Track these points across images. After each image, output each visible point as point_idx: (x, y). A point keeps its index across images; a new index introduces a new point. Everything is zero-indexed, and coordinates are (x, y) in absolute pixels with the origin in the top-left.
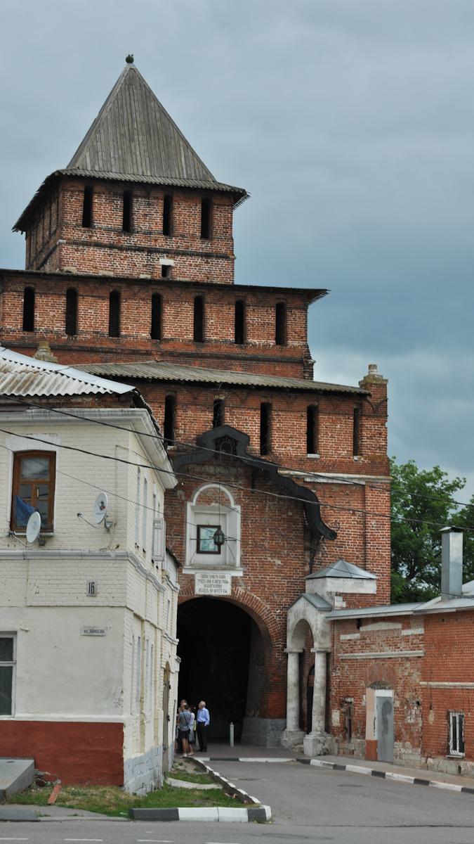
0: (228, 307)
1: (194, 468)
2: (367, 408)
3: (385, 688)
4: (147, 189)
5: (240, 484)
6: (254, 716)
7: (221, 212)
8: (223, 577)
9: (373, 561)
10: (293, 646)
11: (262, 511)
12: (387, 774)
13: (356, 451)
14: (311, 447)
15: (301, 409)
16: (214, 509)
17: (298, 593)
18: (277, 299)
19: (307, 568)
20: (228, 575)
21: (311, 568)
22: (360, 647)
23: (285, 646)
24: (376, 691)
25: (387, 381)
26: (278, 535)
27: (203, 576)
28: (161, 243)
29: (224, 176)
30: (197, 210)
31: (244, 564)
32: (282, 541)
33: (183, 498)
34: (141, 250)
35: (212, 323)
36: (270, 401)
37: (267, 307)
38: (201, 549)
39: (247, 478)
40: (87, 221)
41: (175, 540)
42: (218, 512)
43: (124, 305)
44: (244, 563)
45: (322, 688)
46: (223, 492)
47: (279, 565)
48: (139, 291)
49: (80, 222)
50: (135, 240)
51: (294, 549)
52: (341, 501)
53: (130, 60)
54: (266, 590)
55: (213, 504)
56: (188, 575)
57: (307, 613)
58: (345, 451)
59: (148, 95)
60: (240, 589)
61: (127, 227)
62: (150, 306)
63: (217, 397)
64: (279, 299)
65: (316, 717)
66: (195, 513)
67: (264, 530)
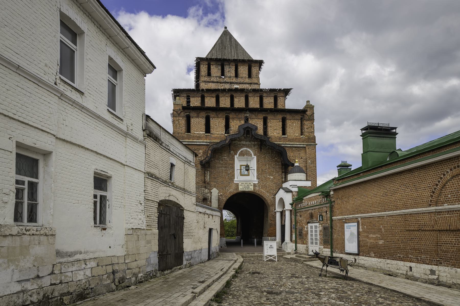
4: (229, 61)
8: (250, 183)
9: (310, 176)
10: (278, 209)
14: (284, 133)
19: (284, 180)
23: (275, 209)
28: (234, 80)
29: (255, 57)
34: (228, 83)
40: (209, 74)
43: (221, 99)
46: (249, 151)
49: (206, 75)
52: (296, 153)
59: (231, 37)
67: (266, 165)
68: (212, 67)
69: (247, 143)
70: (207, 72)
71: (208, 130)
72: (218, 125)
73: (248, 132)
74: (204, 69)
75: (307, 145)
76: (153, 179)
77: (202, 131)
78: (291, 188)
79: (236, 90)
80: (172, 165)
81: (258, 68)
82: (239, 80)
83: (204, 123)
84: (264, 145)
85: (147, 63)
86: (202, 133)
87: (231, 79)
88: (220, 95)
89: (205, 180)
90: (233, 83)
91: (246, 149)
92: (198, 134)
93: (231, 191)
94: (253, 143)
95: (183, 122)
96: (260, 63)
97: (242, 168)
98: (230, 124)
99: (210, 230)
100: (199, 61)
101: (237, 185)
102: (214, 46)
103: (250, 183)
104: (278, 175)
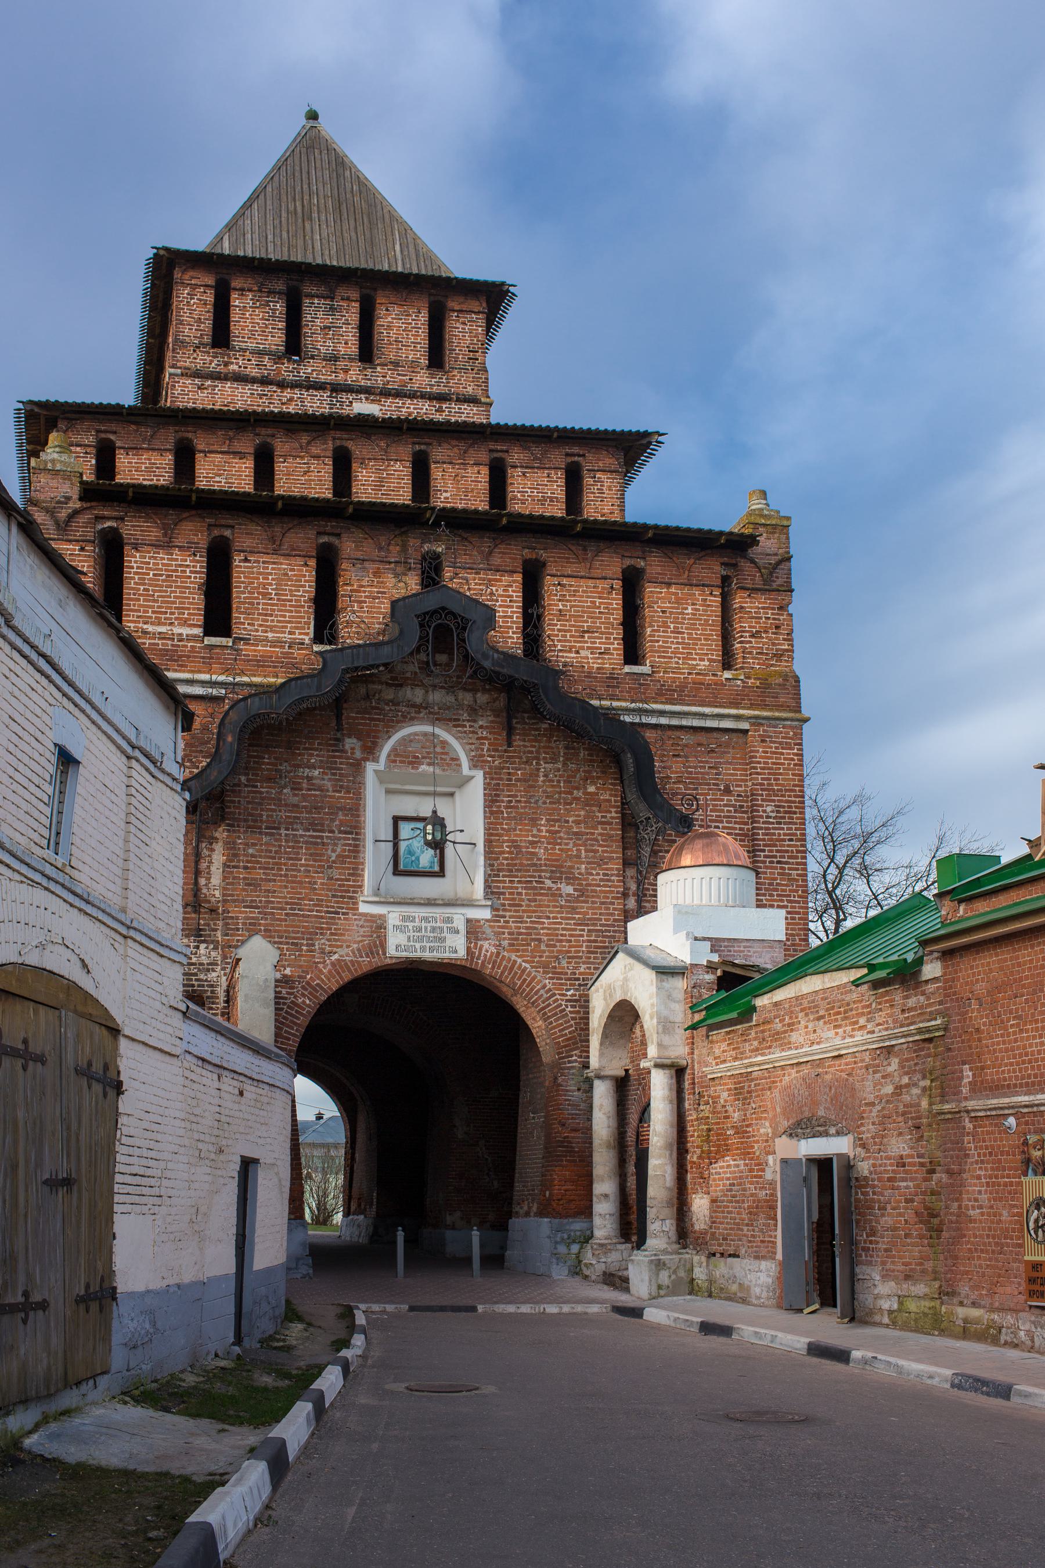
0: (476, 469)
1: (381, 691)
3: (826, 1134)
4: (332, 278)
5: (481, 727)
6: (527, 1214)
7: (464, 323)
8: (449, 920)
11: (529, 781)
12: (856, 1354)
13: (727, 662)
14: (632, 653)
15: (609, 573)
16: (424, 774)
17: (610, 944)
18: (567, 455)
19: (632, 903)
20: (459, 917)
21: (639, 901)
22: (755, 1043)
24: (803, 1142)
25: (788, 518)
26: (568, 833)
27: (405, 919)
28: (355, 375)
29: (460, 264)
31: (492, 893)
32: (575, 845)
33: (358, 754)
34: (320, 386)
35: (446, 498)
36: (543, 555)
37: (549, 468)
38: (401, 867)
39: (496, 713)
40: (221, 336)
41: (342, 842)
42: (431, 789)
45: (668, 1146)
46: (444, 743)
47: (569, 895)
48: (309, 443)
49: (207, 339)
50: (310, 370)
51: (601, 862)
53: (313, 116)
54: (543, 947)
55: (424, 768)
56: (372, 916)
57: (631, 985)
58: (704, 659)
60: (486, 945)
61: (294, 345)
62: (330, 468)
64: (573, 455)
65: (654, 1210)
66: (388, 792)
67: (534, 822)
68: (236, 300)
69: (437, 697)
70: (207, 325)
71: (218, 617)
72: (275, 589)
73: (441, 632)
74: (193, 306)
75: (756, 721)
77: (185, 623)
79: (365, 425)
80: (66, 760)
81: (482, 322)
82: (380, 376)
83: (200, 578)
84: (528, 703)
86: (185, 631)
88: (281, 445)
90: (349, 389)
91: (428, 729)
92: (162, 636)
93: (341, 957)
94: (467, 698)
98: (343, 590)
99: (248, 1165)
100: (167, 268)
101: (378, 926)
104: (607, 875)
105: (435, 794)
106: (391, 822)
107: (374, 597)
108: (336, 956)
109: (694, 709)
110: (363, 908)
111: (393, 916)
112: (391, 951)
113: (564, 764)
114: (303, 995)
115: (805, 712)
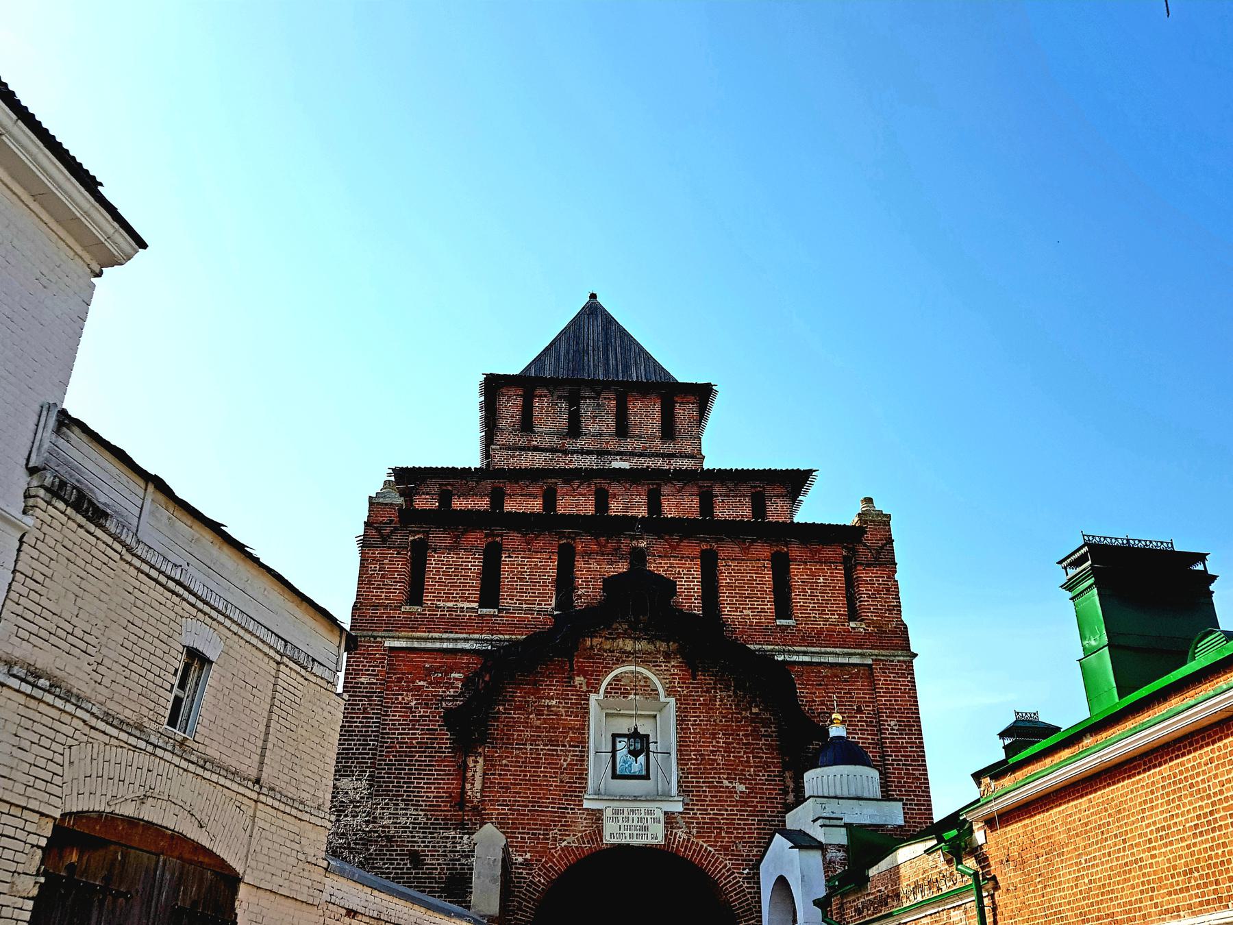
2: (864, 554)
8: (651, 812)
11: (709, 705)
13: (853, 614)
14: (783, 607)
19: (791, 798)
29: (683, 375)
30: (656, 409)
33: (585, 688)
40: (527, 425)
44: (683, 790)
51: (765, 766)
53: (593, 296)
58: (835, 615)
60: (679, 832)
61: (574, 429)
63: (634, 543)
69: (641, 645)
71: (490, 593)
76: (38, 693)
78: (819, 833)
79: (619, 474)
80: (196, 659)
84: (704, 647)
85: (111, 227)
86: (466, 605)
87: (604, 439)
88: (561, 488)
89: (463, 792)
90: (609, 453)
91: (632, 668)
92: (450, 609)
94: (663, 646)
95: (398, 564)
96: (702, 394)
97: (619, 746)
102: (551, 345)
103: (651, 812)
105: (636, 716)
106: (610, 738)
107: (593, 574)
108: (565, 843)
109: (828, 650)
110: (586, 804)
111: (608, 809)
112: (607, 839)
113: (735, 692)
114: (539, 875)
115: (913, 649)
